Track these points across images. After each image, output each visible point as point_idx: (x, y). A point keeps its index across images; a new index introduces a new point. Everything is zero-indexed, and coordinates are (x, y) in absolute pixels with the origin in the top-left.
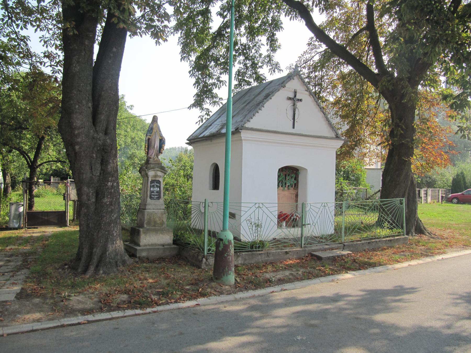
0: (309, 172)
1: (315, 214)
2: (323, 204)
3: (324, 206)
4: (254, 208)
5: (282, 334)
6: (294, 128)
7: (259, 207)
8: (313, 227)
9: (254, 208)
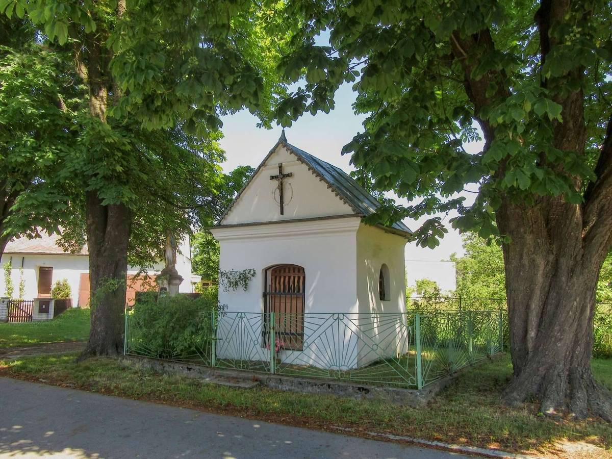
0: (387, 264)
1: (329, 332)
2: (240, 314)
3: (241, 317)
4: (331, 320)
5: (18, 433)
6: (282, 213)
7: (338, 318)
8: (226, 344)
9: (331, 320)
